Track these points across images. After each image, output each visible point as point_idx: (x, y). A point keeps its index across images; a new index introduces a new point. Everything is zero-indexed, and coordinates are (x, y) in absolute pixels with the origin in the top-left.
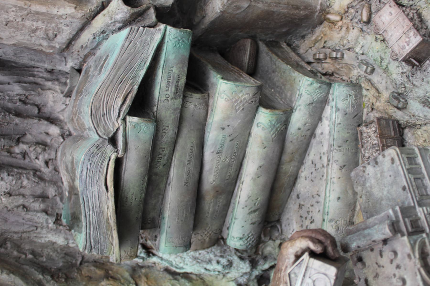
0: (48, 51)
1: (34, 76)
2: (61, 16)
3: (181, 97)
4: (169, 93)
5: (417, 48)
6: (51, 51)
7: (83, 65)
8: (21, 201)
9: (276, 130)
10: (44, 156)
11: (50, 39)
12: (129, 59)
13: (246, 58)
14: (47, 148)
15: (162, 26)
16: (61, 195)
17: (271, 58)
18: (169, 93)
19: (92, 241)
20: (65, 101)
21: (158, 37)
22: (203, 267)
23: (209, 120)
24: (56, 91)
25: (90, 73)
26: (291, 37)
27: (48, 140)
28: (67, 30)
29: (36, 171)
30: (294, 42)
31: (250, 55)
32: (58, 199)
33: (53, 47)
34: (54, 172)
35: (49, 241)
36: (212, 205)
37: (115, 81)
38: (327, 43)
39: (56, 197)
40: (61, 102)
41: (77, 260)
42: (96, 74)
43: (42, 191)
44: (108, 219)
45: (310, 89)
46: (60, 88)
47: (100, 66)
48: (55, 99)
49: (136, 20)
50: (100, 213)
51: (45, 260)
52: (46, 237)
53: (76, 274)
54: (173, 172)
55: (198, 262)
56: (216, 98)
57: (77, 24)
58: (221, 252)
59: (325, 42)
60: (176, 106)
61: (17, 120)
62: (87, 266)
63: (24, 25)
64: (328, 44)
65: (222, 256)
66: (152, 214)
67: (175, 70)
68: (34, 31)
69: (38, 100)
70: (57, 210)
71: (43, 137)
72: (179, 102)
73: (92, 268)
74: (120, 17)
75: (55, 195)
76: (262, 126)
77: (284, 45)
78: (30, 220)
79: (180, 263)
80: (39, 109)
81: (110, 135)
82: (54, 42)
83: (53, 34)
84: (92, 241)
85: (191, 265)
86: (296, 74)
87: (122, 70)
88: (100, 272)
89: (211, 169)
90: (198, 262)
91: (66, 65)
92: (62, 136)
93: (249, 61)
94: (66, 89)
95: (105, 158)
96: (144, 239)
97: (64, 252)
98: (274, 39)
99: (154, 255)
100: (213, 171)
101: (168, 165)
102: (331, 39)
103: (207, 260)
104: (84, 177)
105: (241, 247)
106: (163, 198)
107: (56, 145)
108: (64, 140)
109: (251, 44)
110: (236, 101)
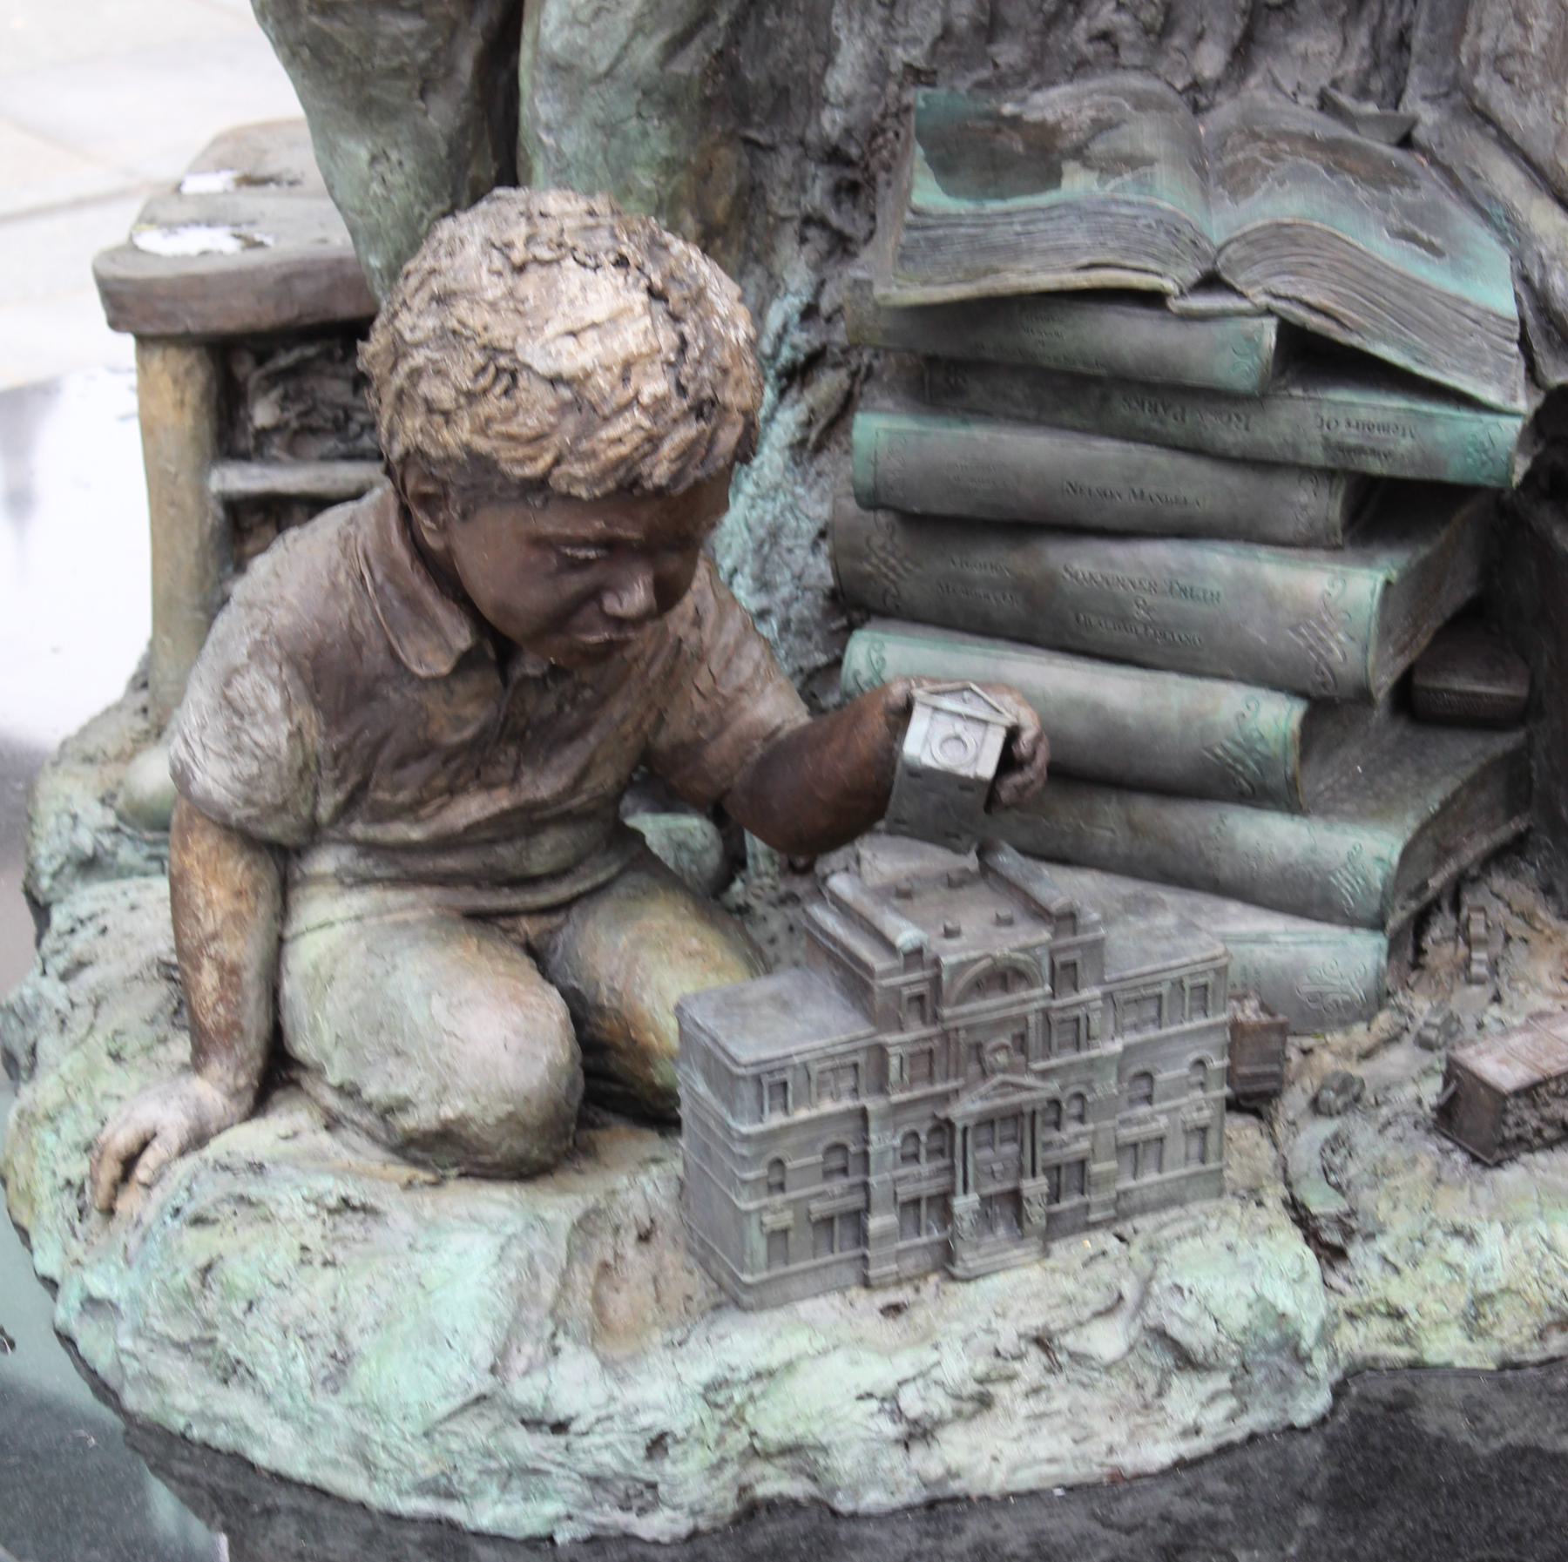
0: (1464, 49)
3: (1330, 464)
4: (1343, 428)
5: (1482, 1091)
6: (1464, 61)
7: (1424, 155)
9: (1236, 759)
10: (1127, 30)
11: (1498, 61)
12: (1429, 319)
13: (1465, 683)
14: (1153, 38)
15: (1525, 404)
16: (999, 84)
17: (1466, 762)
18: (1343, 428)
19: (940, 232)
20: (1306, 93)
21: (1490, 394)
22: (744, 561)
23: (1263, 552)
24: (1338, 63)
25: (1395, 190)
26: (1548, 847)
27: (1178, 40)
28: (1523, 118)
30: (1533, 864)
31: (1475, 695)
32: (984, 73)
33: (1475, 69)
34: (1074, 59)
35: (838, 41)
36: (994, 575)
37: (1371, 284)
38: (1522, 945)
39: (990, 65)
40: (1301, 79)
41: (760, 127)
42: (1392, 219)
43: (1012, 22)
44: (996, 271)
45: (1366, 860)
46: (1352, 76)
47: (1416, 229)
48: (1312, 59)
49: (1552, 328)
50: (1014, 252)
51: (768, 23)
52: (850, 30)
53: (719, 128)
54: (1108, 450)
55: (761, 546)
56: (1329, 567)
58: (802, 621)
59: (1525, 941)
60: (1305, 449)
62: (739, 164)
64: (1517, 949)
65: (785, 626)
66: (977, 390)
67: (1405, 444)
68: (1520, 18)
70: (946, 71)
71: (1189, 23)
72: (1317, 456)
73: (734, 182)
75: (996, 65)
76: (1248, 714)
77: (1518, 824)
79: (757, 485)
81: (1226, 277)
82: (1491, 69)
83: (1513, 74)
84: (940, 232)
85: (752, 521)
86: (1411, 823)
87: (1401, 302)
88: (720, 207)
89: (1112, 563)
90: (761, 546)
91: (1425, 98)
92: (1196, 86)
93: (1455, 693)
94: (1345, 99)
95: (1164, 262)
96: (840, 357)
97: (791, 86)
98: (1537, 786)
99: (782, 393)
100: (1109, 572)
102: (1531, 953)
103: (767, 576)
104: (1113, 209)
105: (850, 675)
106: (1023, 421)
107: (1163, 67)
108: (1180, 93)
109: (1513, 699)
110: (1322, 624)
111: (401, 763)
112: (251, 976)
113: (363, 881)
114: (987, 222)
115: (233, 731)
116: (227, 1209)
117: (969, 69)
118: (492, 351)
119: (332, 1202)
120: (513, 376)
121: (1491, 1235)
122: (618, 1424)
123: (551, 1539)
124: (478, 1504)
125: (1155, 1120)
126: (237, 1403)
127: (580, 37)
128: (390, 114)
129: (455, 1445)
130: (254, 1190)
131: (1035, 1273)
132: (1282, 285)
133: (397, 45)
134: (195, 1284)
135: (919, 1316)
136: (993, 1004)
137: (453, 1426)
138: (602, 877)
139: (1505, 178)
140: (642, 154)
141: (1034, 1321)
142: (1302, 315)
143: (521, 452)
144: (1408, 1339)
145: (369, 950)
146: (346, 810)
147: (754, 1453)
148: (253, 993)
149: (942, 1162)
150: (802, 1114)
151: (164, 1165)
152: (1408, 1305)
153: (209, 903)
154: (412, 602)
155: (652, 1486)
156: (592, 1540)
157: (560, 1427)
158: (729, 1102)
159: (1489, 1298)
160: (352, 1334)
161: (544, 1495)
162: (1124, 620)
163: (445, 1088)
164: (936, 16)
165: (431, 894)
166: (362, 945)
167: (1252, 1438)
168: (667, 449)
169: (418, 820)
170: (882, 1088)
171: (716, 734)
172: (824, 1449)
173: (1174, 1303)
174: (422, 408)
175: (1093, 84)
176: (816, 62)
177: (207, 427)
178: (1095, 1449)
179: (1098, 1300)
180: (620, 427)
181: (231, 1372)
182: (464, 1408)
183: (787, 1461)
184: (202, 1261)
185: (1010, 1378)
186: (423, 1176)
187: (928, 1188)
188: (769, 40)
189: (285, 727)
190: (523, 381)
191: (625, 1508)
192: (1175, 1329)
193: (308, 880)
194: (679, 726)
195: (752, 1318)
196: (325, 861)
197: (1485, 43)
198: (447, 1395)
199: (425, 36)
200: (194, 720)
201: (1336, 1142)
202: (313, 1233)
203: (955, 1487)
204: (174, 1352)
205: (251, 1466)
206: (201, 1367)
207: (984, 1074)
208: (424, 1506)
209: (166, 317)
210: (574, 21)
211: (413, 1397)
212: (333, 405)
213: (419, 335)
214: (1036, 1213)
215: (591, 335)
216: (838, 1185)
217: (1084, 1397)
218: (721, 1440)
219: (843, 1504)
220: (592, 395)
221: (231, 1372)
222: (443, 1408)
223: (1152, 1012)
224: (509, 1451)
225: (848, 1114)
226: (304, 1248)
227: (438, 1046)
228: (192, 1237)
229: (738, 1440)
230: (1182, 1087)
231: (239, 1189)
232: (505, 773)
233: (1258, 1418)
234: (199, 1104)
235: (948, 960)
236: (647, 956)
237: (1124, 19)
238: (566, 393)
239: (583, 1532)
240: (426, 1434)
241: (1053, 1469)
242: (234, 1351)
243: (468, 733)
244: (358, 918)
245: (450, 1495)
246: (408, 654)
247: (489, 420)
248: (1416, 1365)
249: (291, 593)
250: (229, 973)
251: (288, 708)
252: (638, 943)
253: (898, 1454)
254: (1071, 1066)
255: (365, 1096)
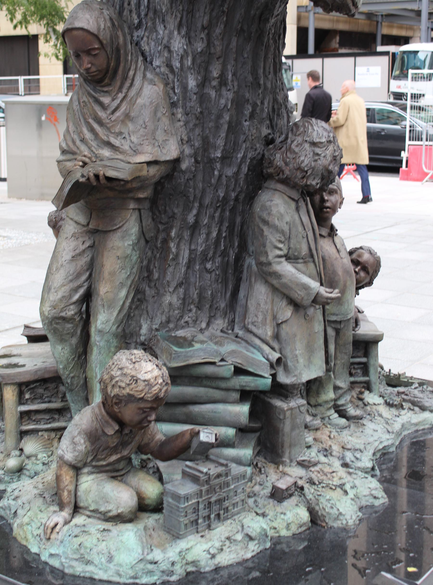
1: (230, 312)
2: (266, 329)
8: (166, 310)
11: (253, 323)
21: (266, 375)
23: (227, 404)
27: (198, 322)
29: (182, 317)
32: (167, 329)
33: (248, 324)
50: (191, 357)
57: (263, 337)
61: (208, 306)
63: (259, 311)
66: (179, 381)
67: (253, 385)
68: (256, 316)
69: (218, 315)
71: (200, 319)
74: (270, 357)
78: (156, 315)
80: (213, 316)
81: (225, 359)
92: (201, 330)
101: (205, 386)
111: (103, 451)
112: (73, 492)
113: (92, 473)
114: (187, 352)
115: (74, 448)
116: (81, 533)
117: (165, 328)
118: (133, 377)
119: (102, 529)
120: (137, 381)
121: (288, 513)
122: (166, 561)
123: (156, 583)
124: (142, 579)
125: (237, 499)
126: (90, 568)
127: (104, 326)
128: (66, 341)
129: (137, 569)
130: (86, 529)
131: (223, 527)
132: (234, 360)
133: (68, 329)
134: (78, 547)
135: (208, 536)
136: (217, 481)
137: (136, 565)
138: (129, 469)
139: (257, 342)
140: (112, 345)
141: (227, 535)
142: (237, 365)
143: (139, 393)
144: (278, 532)
145: (97, 485)
146: (92, 461)
147: (187, 564)
148: (73, 495)
149: (209, 509)
150: (190, 503)
151: (60, 529)
152: (277, 526)
153: (66, 480)
154: (107, 422)
155: (173, 571)
156: (162, 583)
157: (156, 563)
158: (179, 502)
159: (290, 523)
160: (112, 552)
161: (154, 576)
162: (204, 418)
163: (118, 507)
164: (160, 320)
165: (104, 474)
166: (96, 484)
167: (261, 551)
168: (163, 391)
169: (105, 461)
170: (201, 497)
171: (152, 441)
172: (199, 561)
173: (249, 529)
174: (118, 387)
175: (186, 330)
176: (138, 329)
177: (18, 399)
178: (240, 555)
179: (236, 530)
180: (156, 388)
181: (88, 562)
182: (138, 562)
183: (192, 564)
184: (79, 543)
185: (225, 545)
186: (114, 524)
187: (207, 514)
188: (130, 325)
189: (84, 446)
190: (139, 381)
191: (168, 576)
192: (250, 533)
193: (81, 474)
194: (146, 440)
195: (181, 540)
196: (86, 470)
197: (250, 320)
198: (135, 560)
199: (73, 327)
200: (65, 446)
201: (255, 501)
202: (99, 535)
203: (220, 565)
204: (74, 561)
205: (95, 579)
206: (81, 563)
207: (216, 493)
208: (131, 581)
209: (13, 380)
210: (103, 323)
211: (128, 561)
212: (40, 394)
213: (117, 375)
214: (222, 517)
215: (149, 373)
216: (194, 515)
217: (237, 547)
218: (182, 562)
219: (202, 570)
220: (150, 383)
221: (88, 562)
222: (134, 562)
223: (237, 480)
224: (147, 568)
225: (196, 502)
226: (98, 539)
227: (116, 500)
228: (75, 539)
229: (184, 561)
230: (240, 493)
231: (83, 530)
232: (119, 451)
233: (261, 548)
234: (64, 516)
235: (211, 474)
236: (141, 482)
237: (190, 319)
238: (146, 383)
239: (161, 581)
240: (132, 568)
241: (234, 560)
242: (89, 559)
243: (115, 444)
244: (93, 479)
245: (136, 578)
246: (106, 431)
247: (133, 388)
248: (279, 536)
249: (85, 422)
250: (69, 492)
251: (85, 442)
252: (139, 479)
253: (210, 560)
254: (227, 491)
255: (100, 511)
